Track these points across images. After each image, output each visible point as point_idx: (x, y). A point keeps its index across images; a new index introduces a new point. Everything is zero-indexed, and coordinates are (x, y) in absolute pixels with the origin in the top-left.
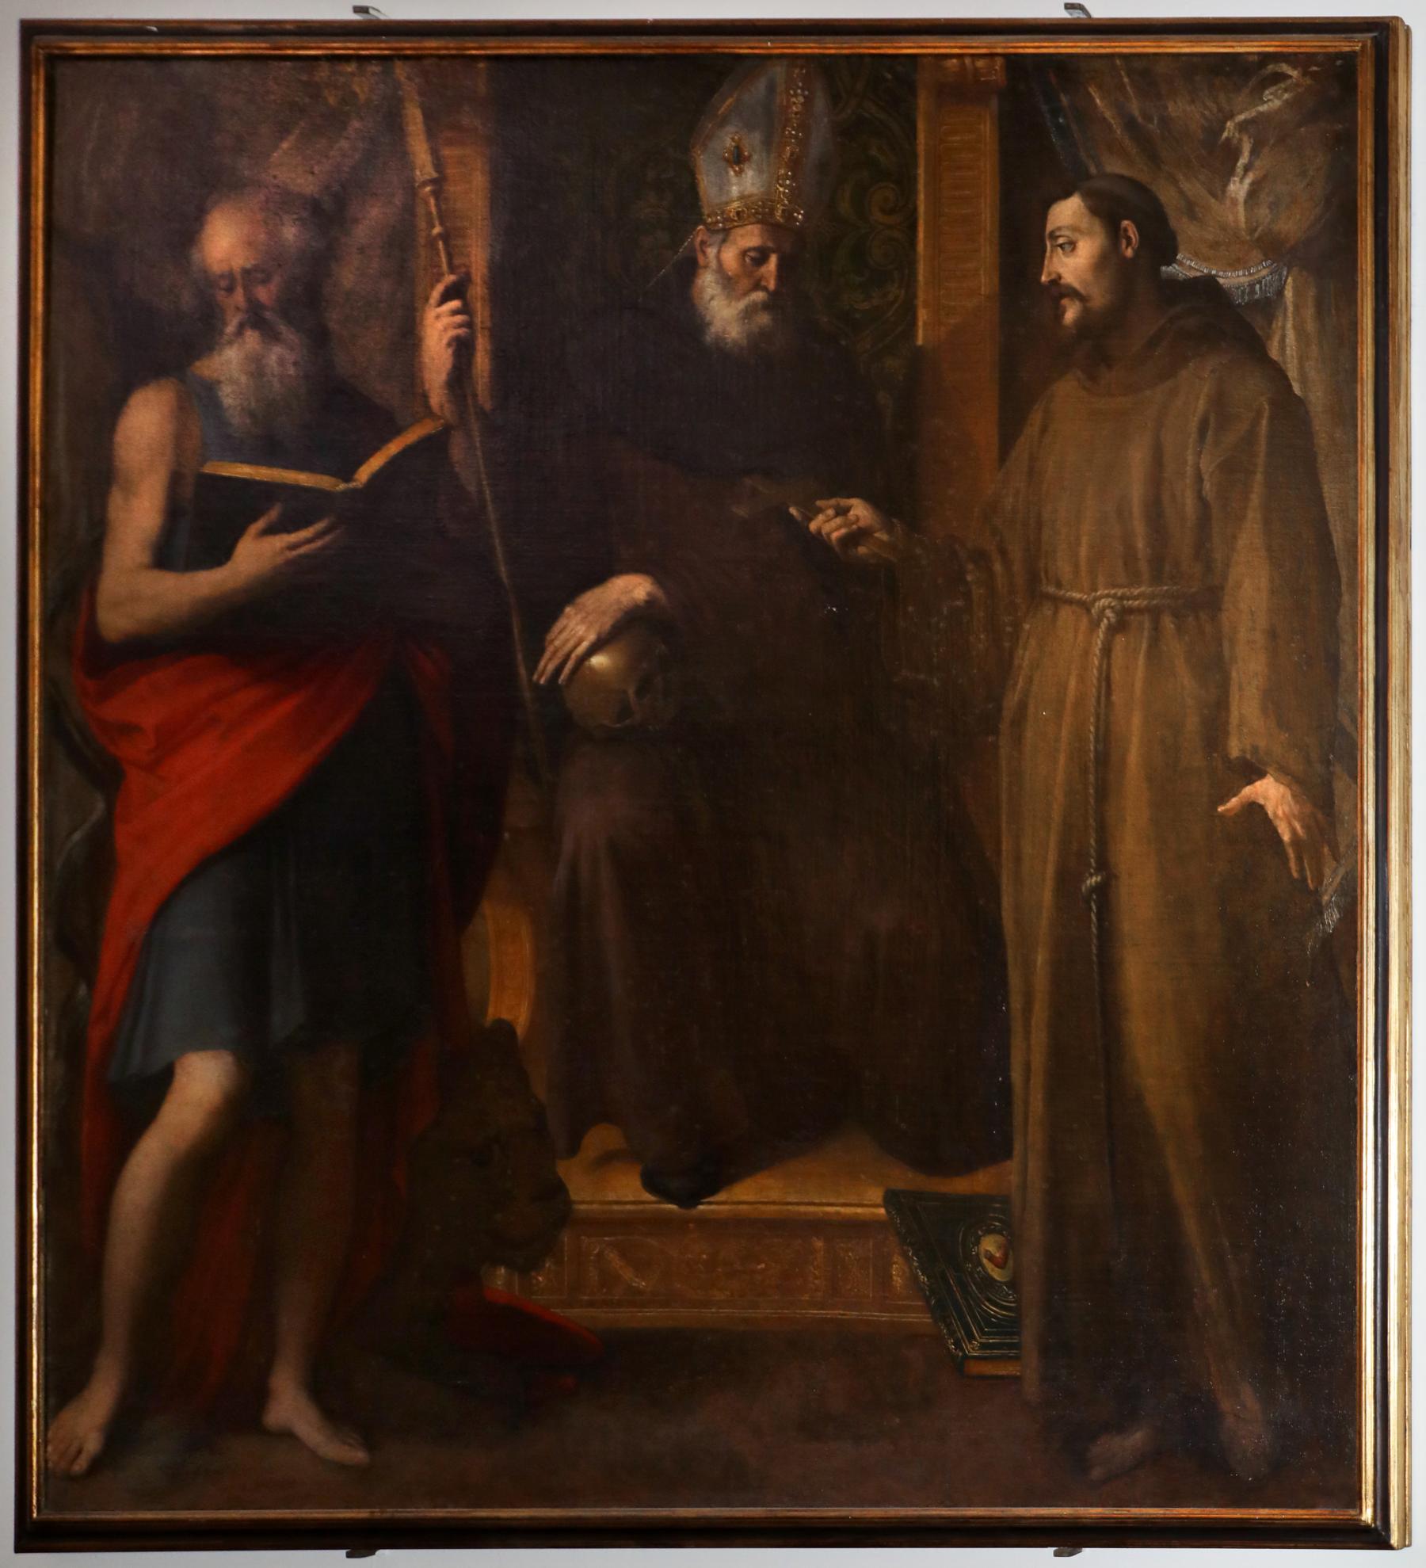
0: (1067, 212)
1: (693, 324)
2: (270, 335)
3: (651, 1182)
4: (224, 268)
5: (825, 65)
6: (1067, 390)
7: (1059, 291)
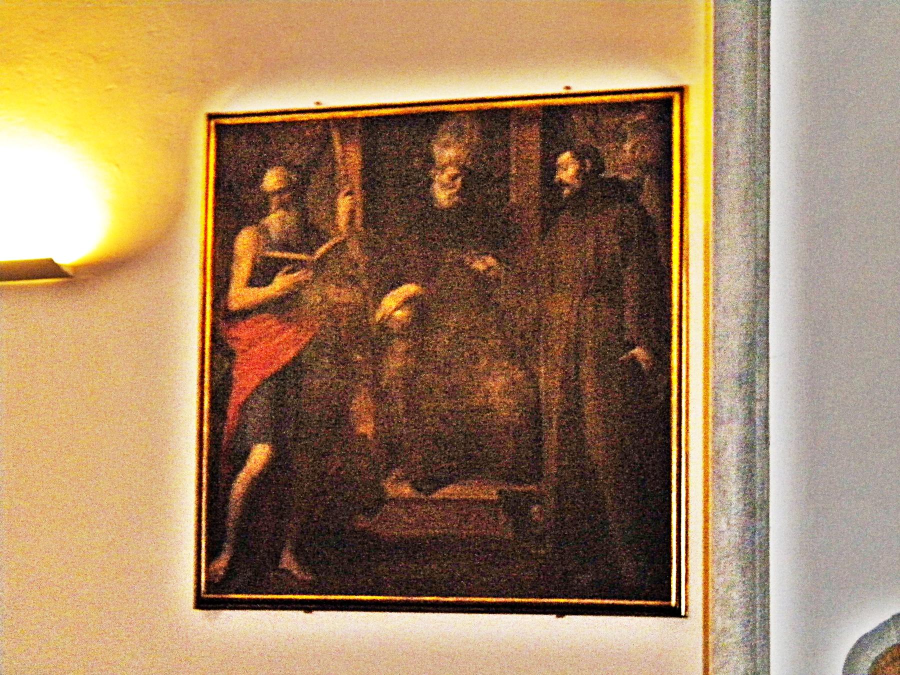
0: (566, 157)
1: (430, 199)
2: (287, 209)
3: (414, 484)
4: (271, 190)
5: (480, 113)
6: (564, 216)
7: (562, 184)
